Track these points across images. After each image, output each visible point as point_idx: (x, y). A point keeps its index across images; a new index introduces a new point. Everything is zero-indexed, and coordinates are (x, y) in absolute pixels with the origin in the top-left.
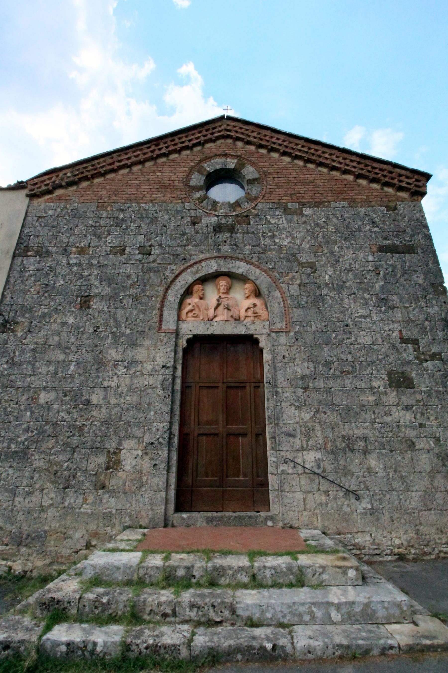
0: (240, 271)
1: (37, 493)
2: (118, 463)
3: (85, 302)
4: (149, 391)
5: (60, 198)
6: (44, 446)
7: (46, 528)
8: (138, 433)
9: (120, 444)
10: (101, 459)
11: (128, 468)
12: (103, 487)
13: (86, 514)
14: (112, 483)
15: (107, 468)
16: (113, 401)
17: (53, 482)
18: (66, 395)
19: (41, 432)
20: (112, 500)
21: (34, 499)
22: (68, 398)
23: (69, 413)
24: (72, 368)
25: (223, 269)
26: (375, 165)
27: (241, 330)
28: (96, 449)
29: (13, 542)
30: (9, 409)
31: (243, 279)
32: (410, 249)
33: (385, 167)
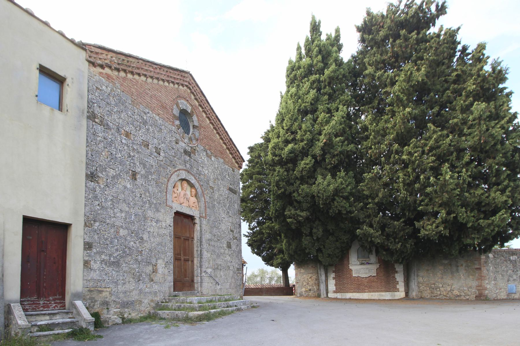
0: (192, 182)
1: (127, 283)
2: (157, 270)
3: (134, 176)
4: (165, 237)
5: (108, 77)
6: (127, 259)
7: (133, 299)
8: (163, 257)
9: (157, 261)
10: (150, 268)
11: (160, 272)
12: (152, 280)
13: (147, 292)
14: (155, 279)
15: (153, 272)
16: (152, 239)
17: (133, 278)
18: (132, 233)
19: (124, 252)
20: (156, 286)
21: (126, 286)
22: (133, 235)
23: (135, 243)
24: (133, 217)
25: (187, 178)
26: (233, 146)
27: (191, 213)
28: (149, 263)
29: (338, 72)
30: (106, 237)
31: (192, 186)
32: (184, 281)
33: (235, 148)
